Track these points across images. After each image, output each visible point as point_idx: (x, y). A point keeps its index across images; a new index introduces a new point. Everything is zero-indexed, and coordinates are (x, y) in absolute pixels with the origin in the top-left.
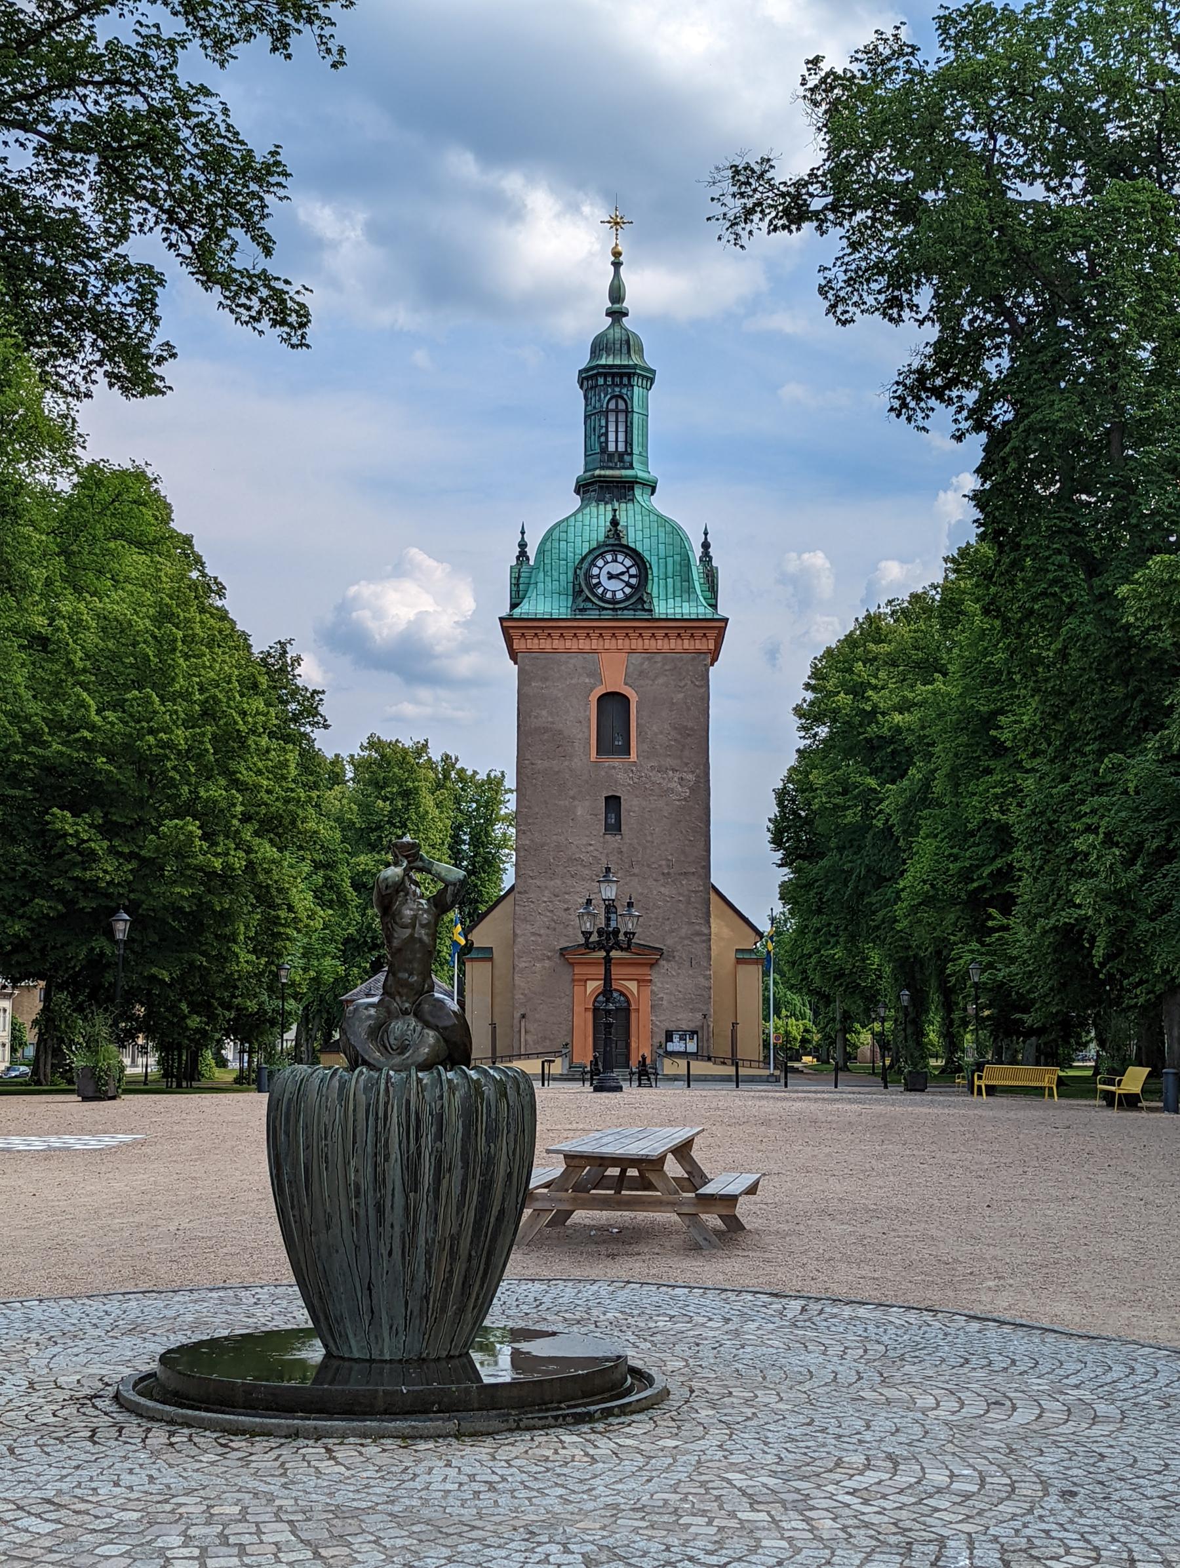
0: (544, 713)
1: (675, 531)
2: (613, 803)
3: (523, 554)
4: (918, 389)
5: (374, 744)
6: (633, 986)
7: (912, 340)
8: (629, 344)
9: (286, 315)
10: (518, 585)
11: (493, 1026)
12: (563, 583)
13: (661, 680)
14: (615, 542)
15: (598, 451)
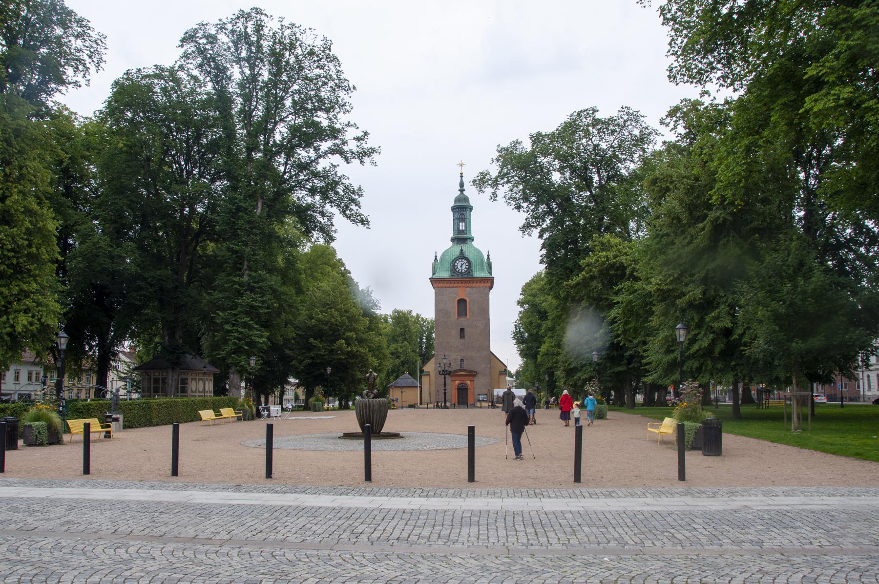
1: (479, 252)
2: (462, 330)
3: (436, 259)
4: (526, 227)
6: (468, 382)
7: (522, 217)
8: (466, 199)
9: (364, 222)
14: (462, 256)
15: (457, 230)
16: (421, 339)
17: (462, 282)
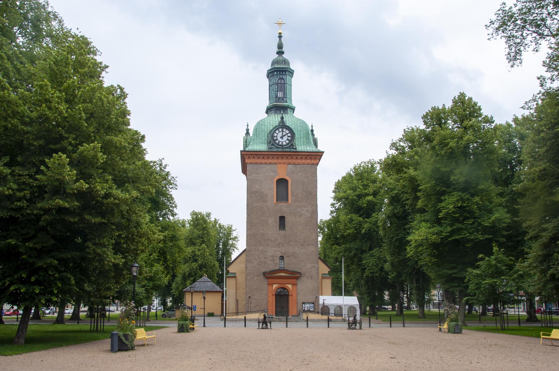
0: (257, 186)
2: (282, 219)
3: (248, 133)
5: (194, 214)
6: (290, 286)
8: (286, 62)
10: (246, 142)
11: (237, 301)
12: (263, 140)
13: (300, 174)
14: (283, 125)
16: (218, 245)
17: (282, 157)
